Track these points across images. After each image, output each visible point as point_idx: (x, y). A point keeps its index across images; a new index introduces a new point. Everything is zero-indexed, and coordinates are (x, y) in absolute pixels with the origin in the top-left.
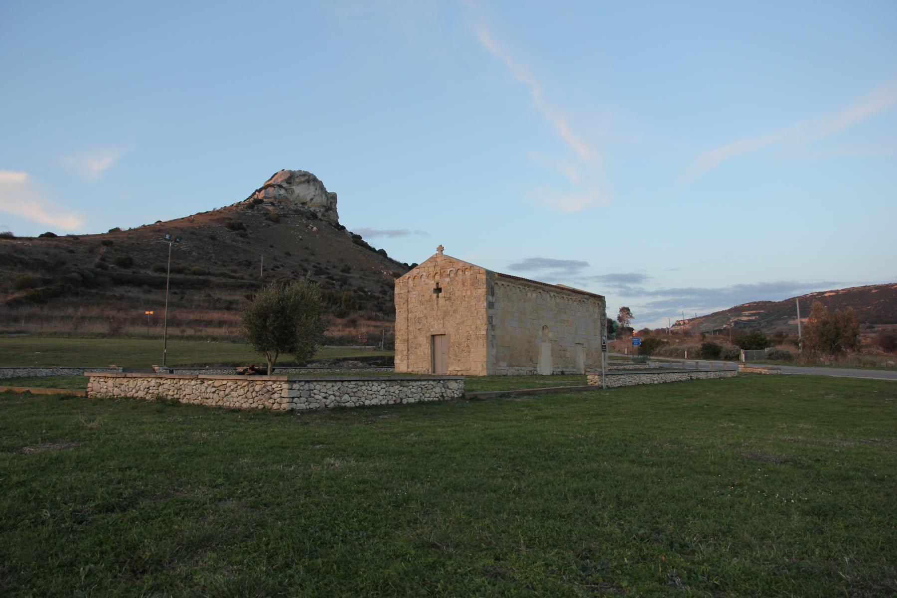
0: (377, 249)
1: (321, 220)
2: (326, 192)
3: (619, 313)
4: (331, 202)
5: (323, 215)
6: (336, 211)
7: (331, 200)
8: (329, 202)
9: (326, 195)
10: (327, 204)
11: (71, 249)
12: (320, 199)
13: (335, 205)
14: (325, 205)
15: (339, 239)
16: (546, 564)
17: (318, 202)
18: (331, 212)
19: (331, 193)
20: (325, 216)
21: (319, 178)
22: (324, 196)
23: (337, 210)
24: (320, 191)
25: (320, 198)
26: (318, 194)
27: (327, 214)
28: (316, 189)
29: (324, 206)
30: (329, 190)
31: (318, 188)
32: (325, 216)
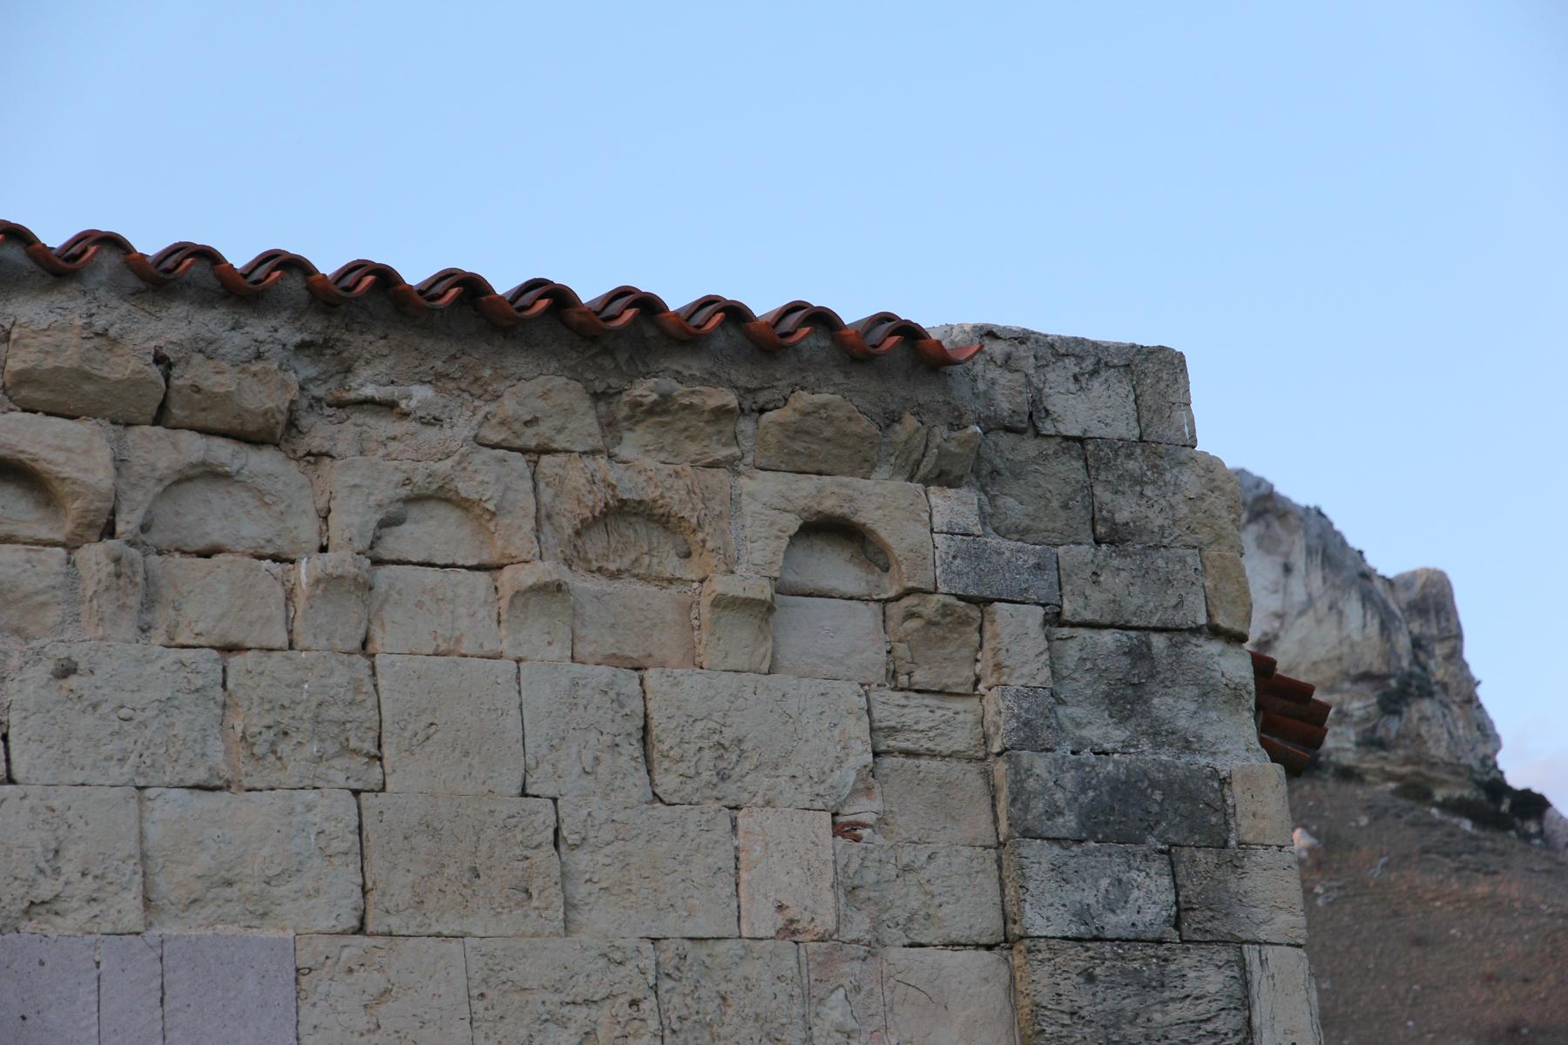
0: (40, 414)
1: (1347, 774)
2: (1366, 575)
3: (1247, 883)
4: (1417, 644)
5: (1371, 742)
6: (1471, 701)
7: (1416, 627)
8: (1403, 642)
9: (1367, 598)
10: (1390, 655)
11: (352, 483)
12: (1330, 632)
13: (1455, 655)
14: (1378, 666)
15: (1482, 888)
16: (849, 1037)
17: (1318, 653)
18: (1427, 706)
19: (1407, 581)
20: (1382, 745)
21: (1295, 489)
22: (1353, 609)
23: (1484, 694)
24: (1317, 579)
25: (1330, 627)
26: (1310, 602)
27: (1394, 725)
28: (1287, 569)
29: (1366, 677)
30: (1388, 560)
31: (1299, 560)
32: (1382, 745)
